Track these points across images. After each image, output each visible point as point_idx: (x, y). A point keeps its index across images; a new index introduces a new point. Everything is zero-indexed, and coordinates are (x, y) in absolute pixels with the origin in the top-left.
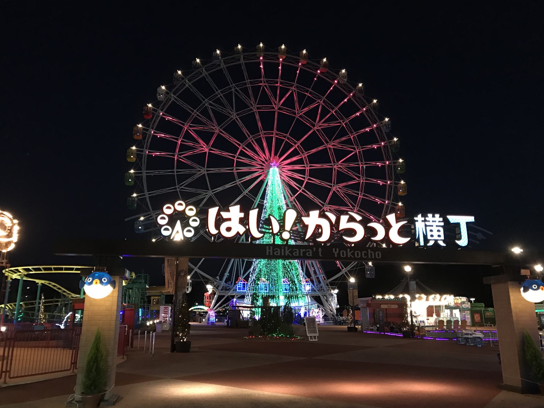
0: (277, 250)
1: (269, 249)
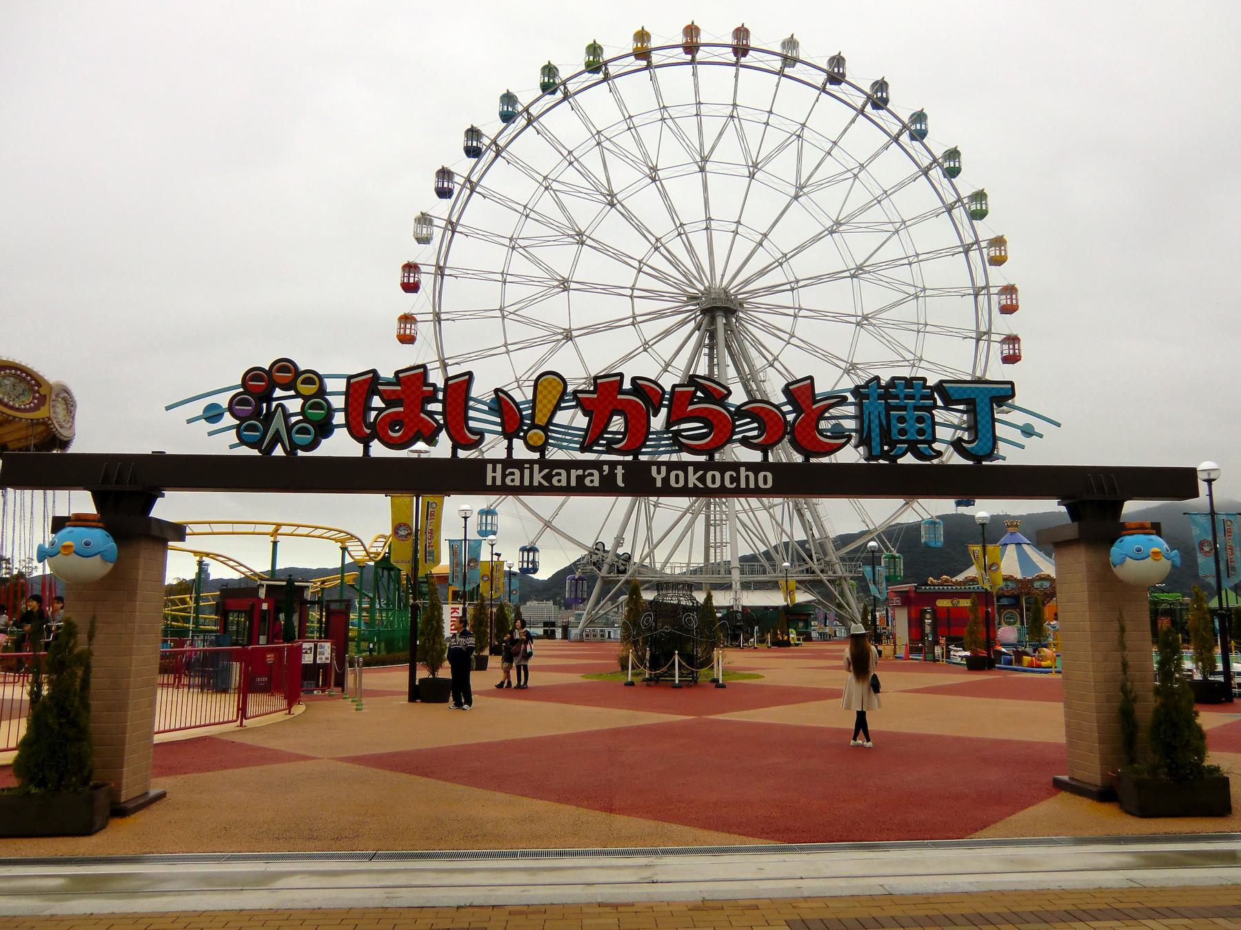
0: (513, 474)
1: (494, 471)
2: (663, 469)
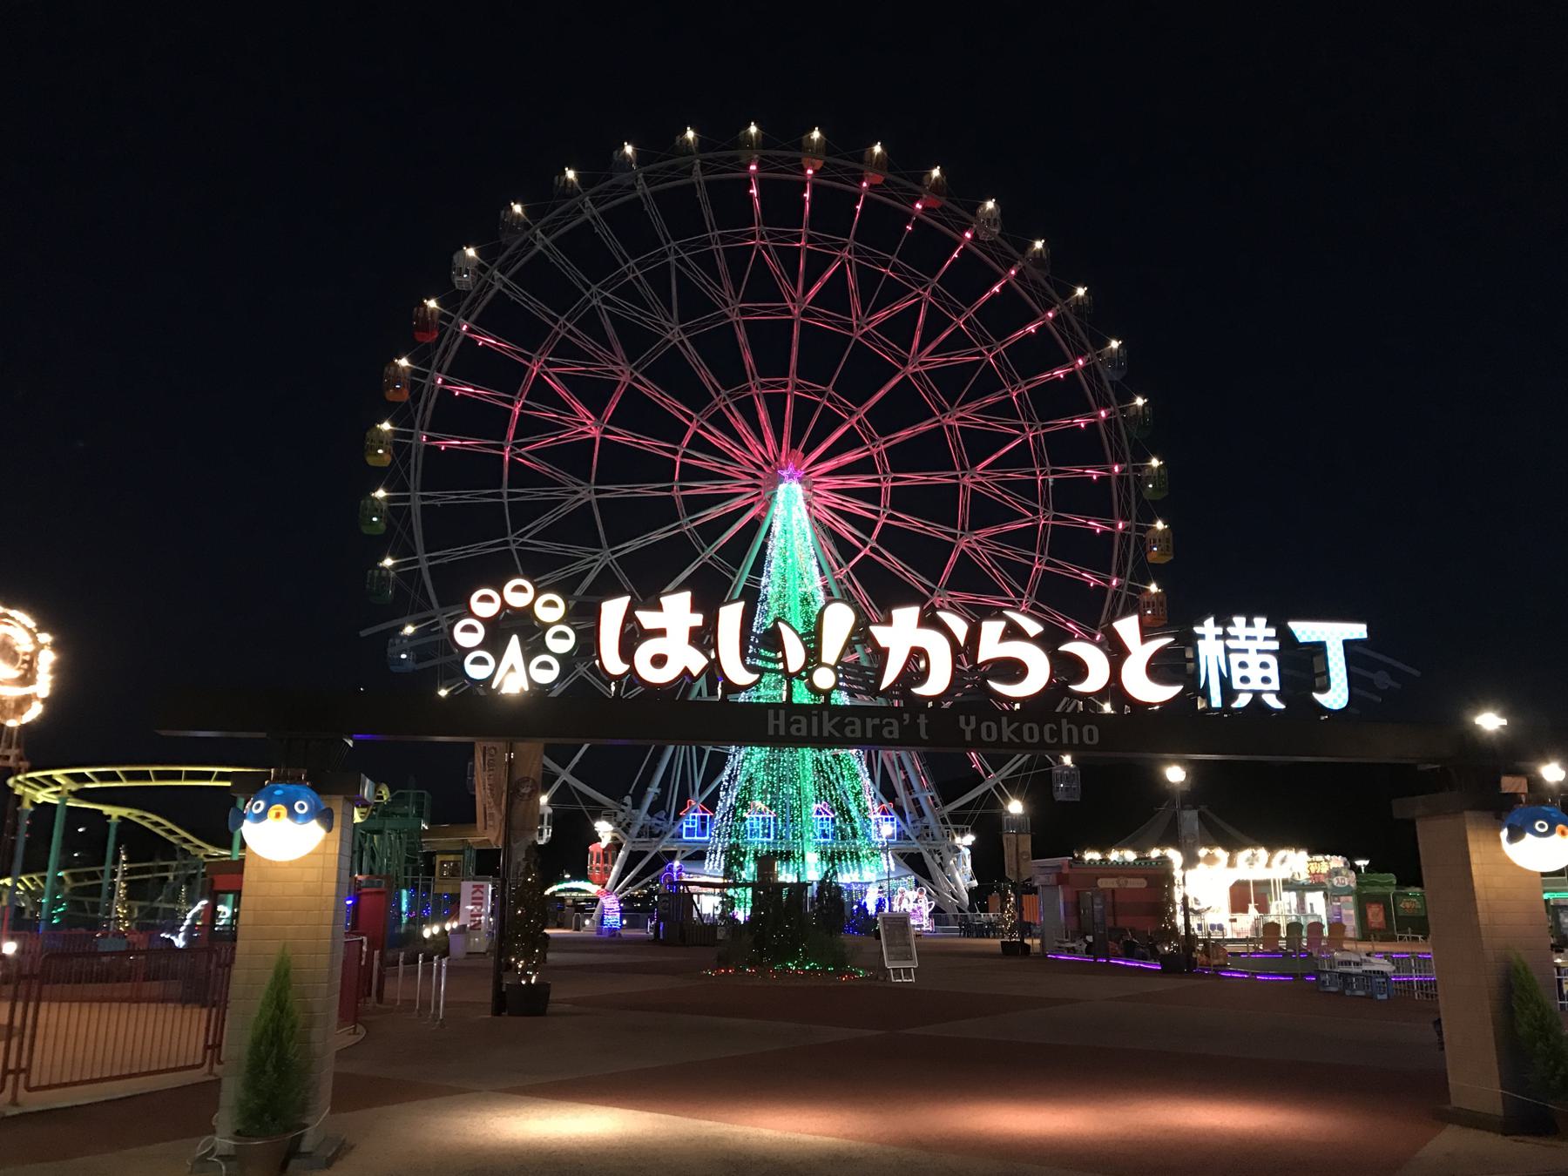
0: (798, 722)
1: (777, 717)
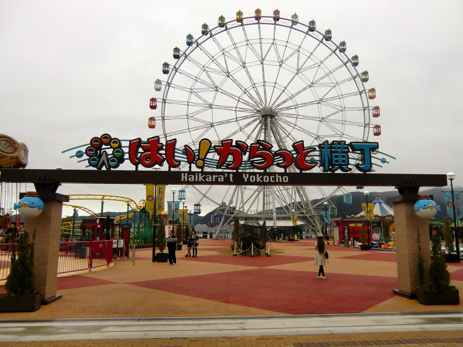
0: (191, 177)
1: (184, 176)
2: (248, 175)
